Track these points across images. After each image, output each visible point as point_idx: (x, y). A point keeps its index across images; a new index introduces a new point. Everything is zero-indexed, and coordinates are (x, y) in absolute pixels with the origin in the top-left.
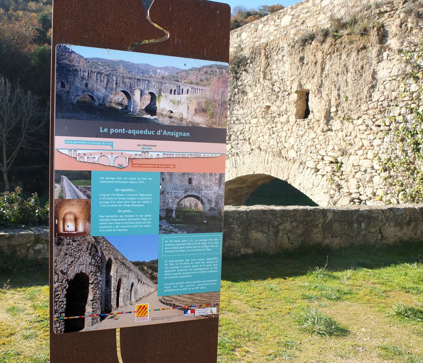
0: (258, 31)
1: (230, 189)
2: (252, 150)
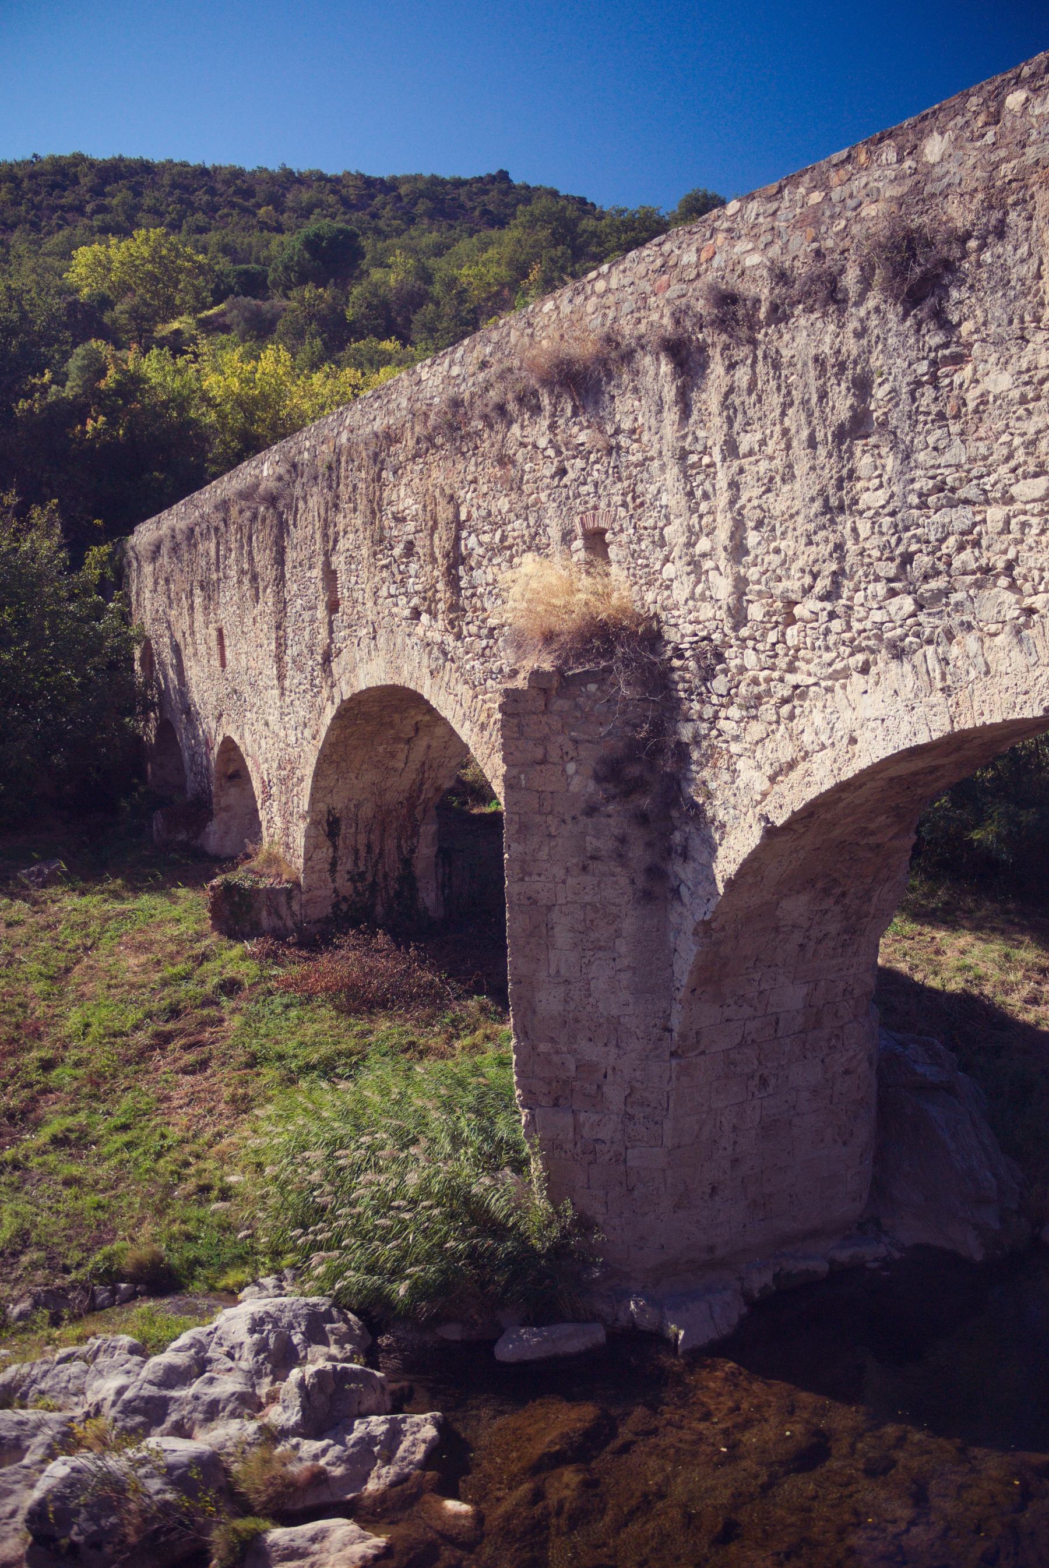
0: (1007, 121)
1: (891, 779)
2: (1030, 611)
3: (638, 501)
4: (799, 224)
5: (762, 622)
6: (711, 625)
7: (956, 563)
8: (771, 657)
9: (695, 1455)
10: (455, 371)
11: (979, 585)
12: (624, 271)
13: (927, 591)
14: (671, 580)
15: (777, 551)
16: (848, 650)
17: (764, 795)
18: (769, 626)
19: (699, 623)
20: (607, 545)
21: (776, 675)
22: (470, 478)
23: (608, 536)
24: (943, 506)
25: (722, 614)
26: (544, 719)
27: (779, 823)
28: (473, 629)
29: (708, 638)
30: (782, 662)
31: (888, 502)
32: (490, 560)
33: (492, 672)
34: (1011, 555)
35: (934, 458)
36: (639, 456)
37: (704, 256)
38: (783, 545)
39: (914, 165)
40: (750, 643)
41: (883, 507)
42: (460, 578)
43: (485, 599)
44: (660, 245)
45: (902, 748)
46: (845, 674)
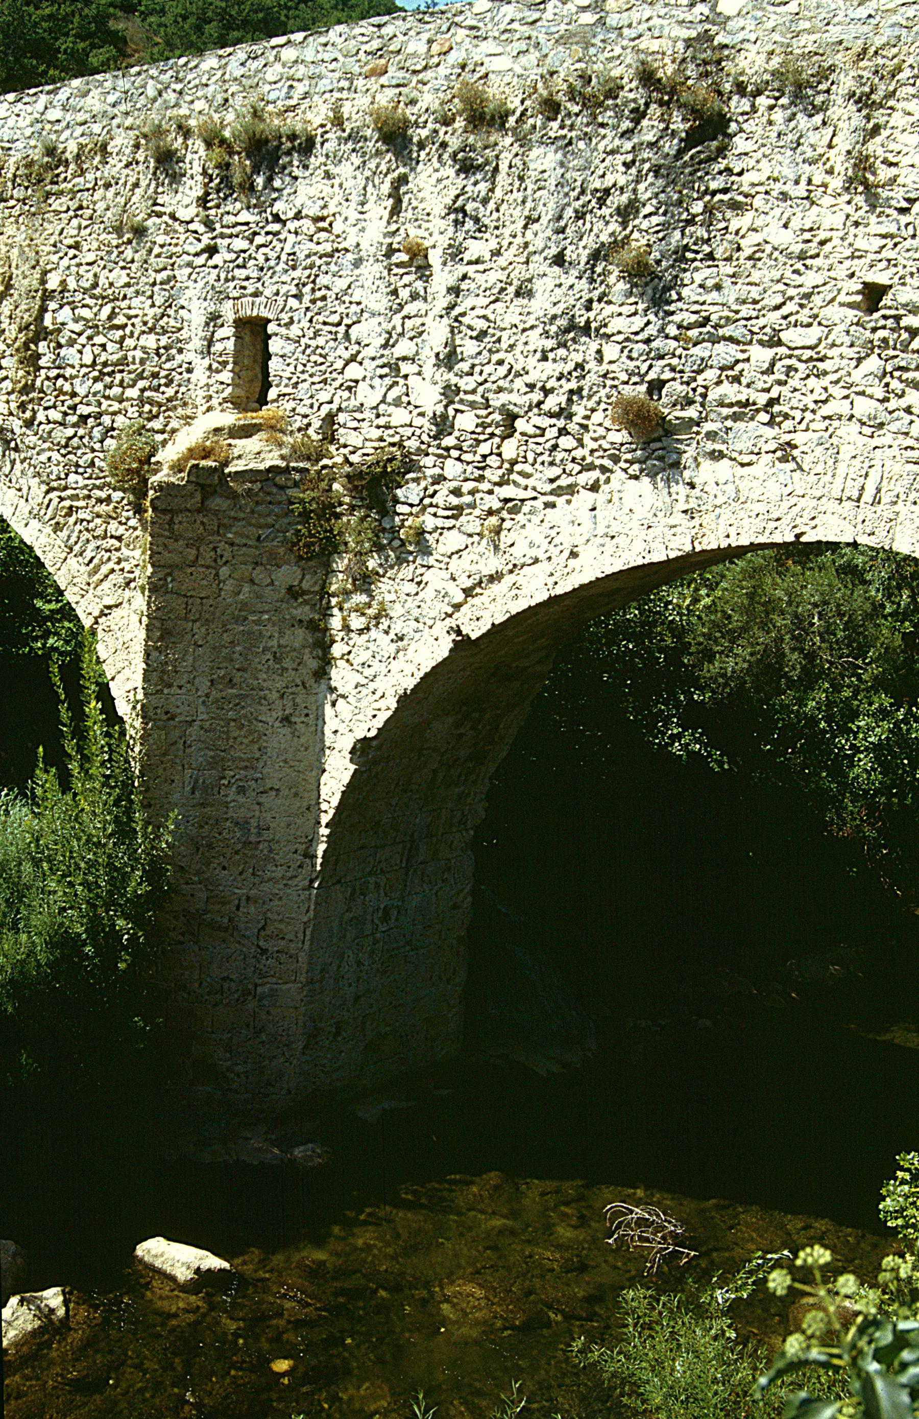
3: (318, 294)
4: (563, 40)
5: (473, 433)
6: (408, 432)
7: (712, 395)
8: (478, 468)
9: (888, 392)
10: (53, 114)
11: (736, 417)
12: (326, 45)
13: (677, 418)
14: (357, 382)
15: (500, 363)
16: (578, 468)
17: (457, 607)
18: (482, 437)
19: (387, 427)
20: (269, 337)
21: (485, 486)
22: (70, 241)
23: (271, 328)
24: (704, 341)
25: (424, 422)
26: (200, 518)
27: (473, 636)
28: (55, 415)
29: (400, 445)
30: (493, 475)
31: (642, 330)
32: (90, 338)
33: (77, 465)
34: (774, 394)
35: (700, 294)
36: (327, 247)
37: (436, 48)
38: (509, 358)
39: (706, 12)
40: (455, 453)
41: (636, 333)
42: (39, 356)
43: (77, 382)
44: (379, 26)
45: (632, 564)
46: (571, 490)
